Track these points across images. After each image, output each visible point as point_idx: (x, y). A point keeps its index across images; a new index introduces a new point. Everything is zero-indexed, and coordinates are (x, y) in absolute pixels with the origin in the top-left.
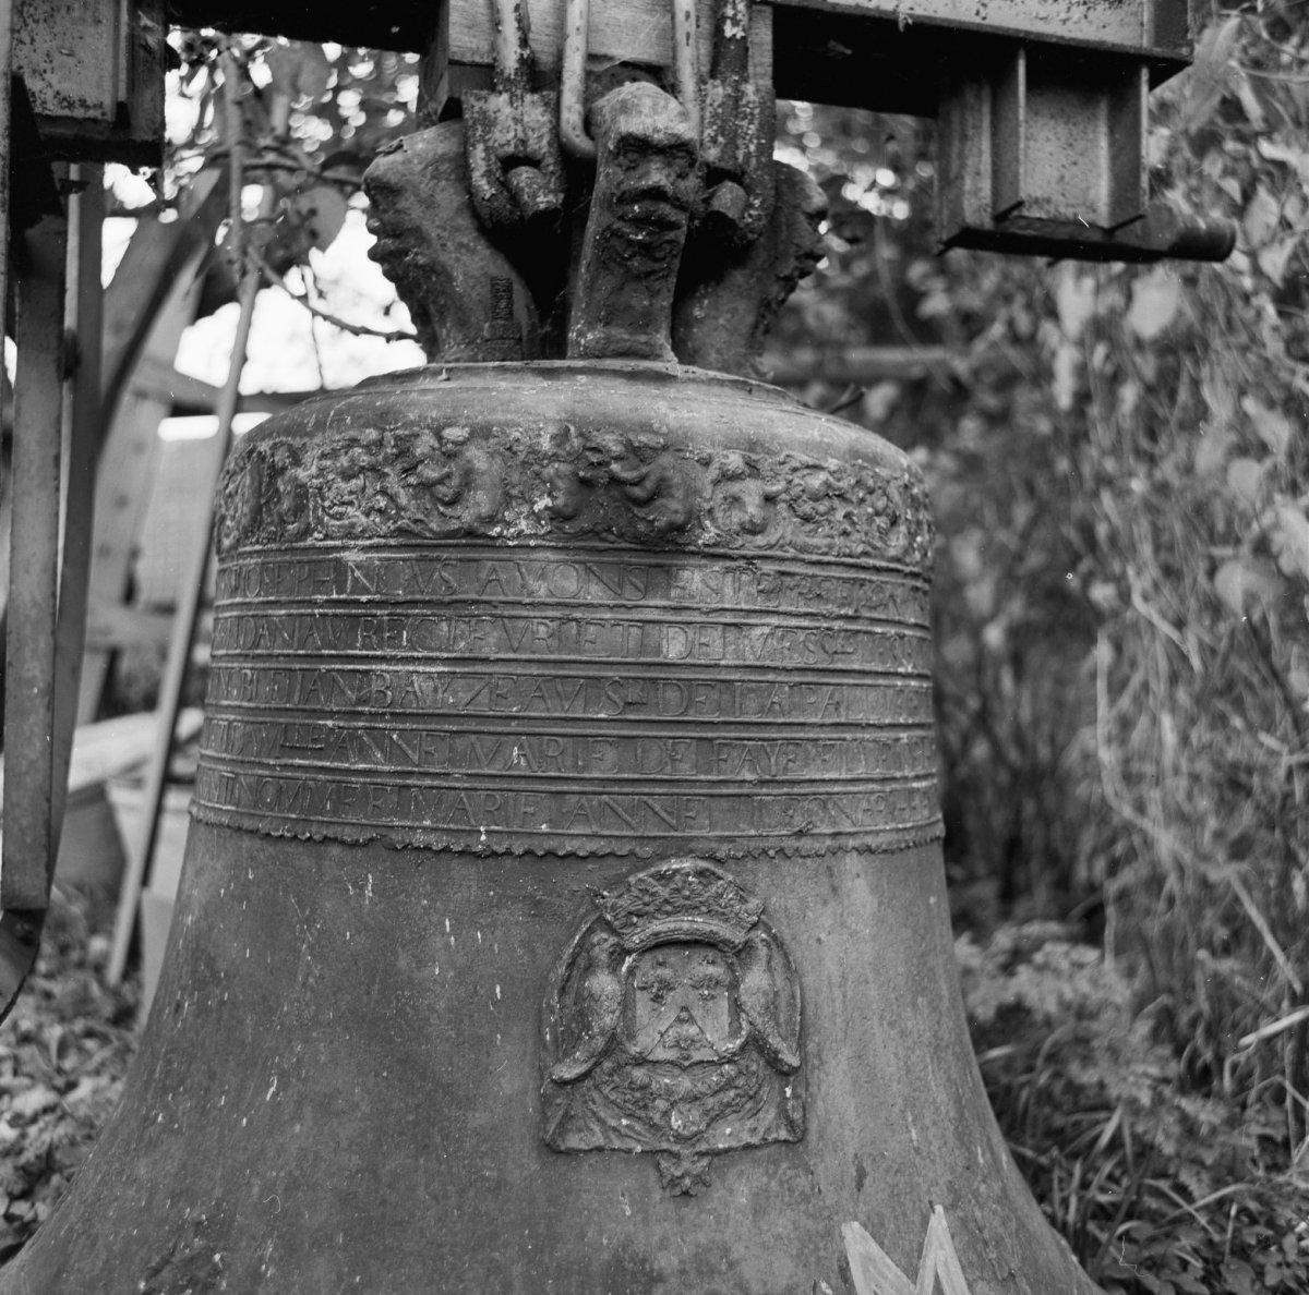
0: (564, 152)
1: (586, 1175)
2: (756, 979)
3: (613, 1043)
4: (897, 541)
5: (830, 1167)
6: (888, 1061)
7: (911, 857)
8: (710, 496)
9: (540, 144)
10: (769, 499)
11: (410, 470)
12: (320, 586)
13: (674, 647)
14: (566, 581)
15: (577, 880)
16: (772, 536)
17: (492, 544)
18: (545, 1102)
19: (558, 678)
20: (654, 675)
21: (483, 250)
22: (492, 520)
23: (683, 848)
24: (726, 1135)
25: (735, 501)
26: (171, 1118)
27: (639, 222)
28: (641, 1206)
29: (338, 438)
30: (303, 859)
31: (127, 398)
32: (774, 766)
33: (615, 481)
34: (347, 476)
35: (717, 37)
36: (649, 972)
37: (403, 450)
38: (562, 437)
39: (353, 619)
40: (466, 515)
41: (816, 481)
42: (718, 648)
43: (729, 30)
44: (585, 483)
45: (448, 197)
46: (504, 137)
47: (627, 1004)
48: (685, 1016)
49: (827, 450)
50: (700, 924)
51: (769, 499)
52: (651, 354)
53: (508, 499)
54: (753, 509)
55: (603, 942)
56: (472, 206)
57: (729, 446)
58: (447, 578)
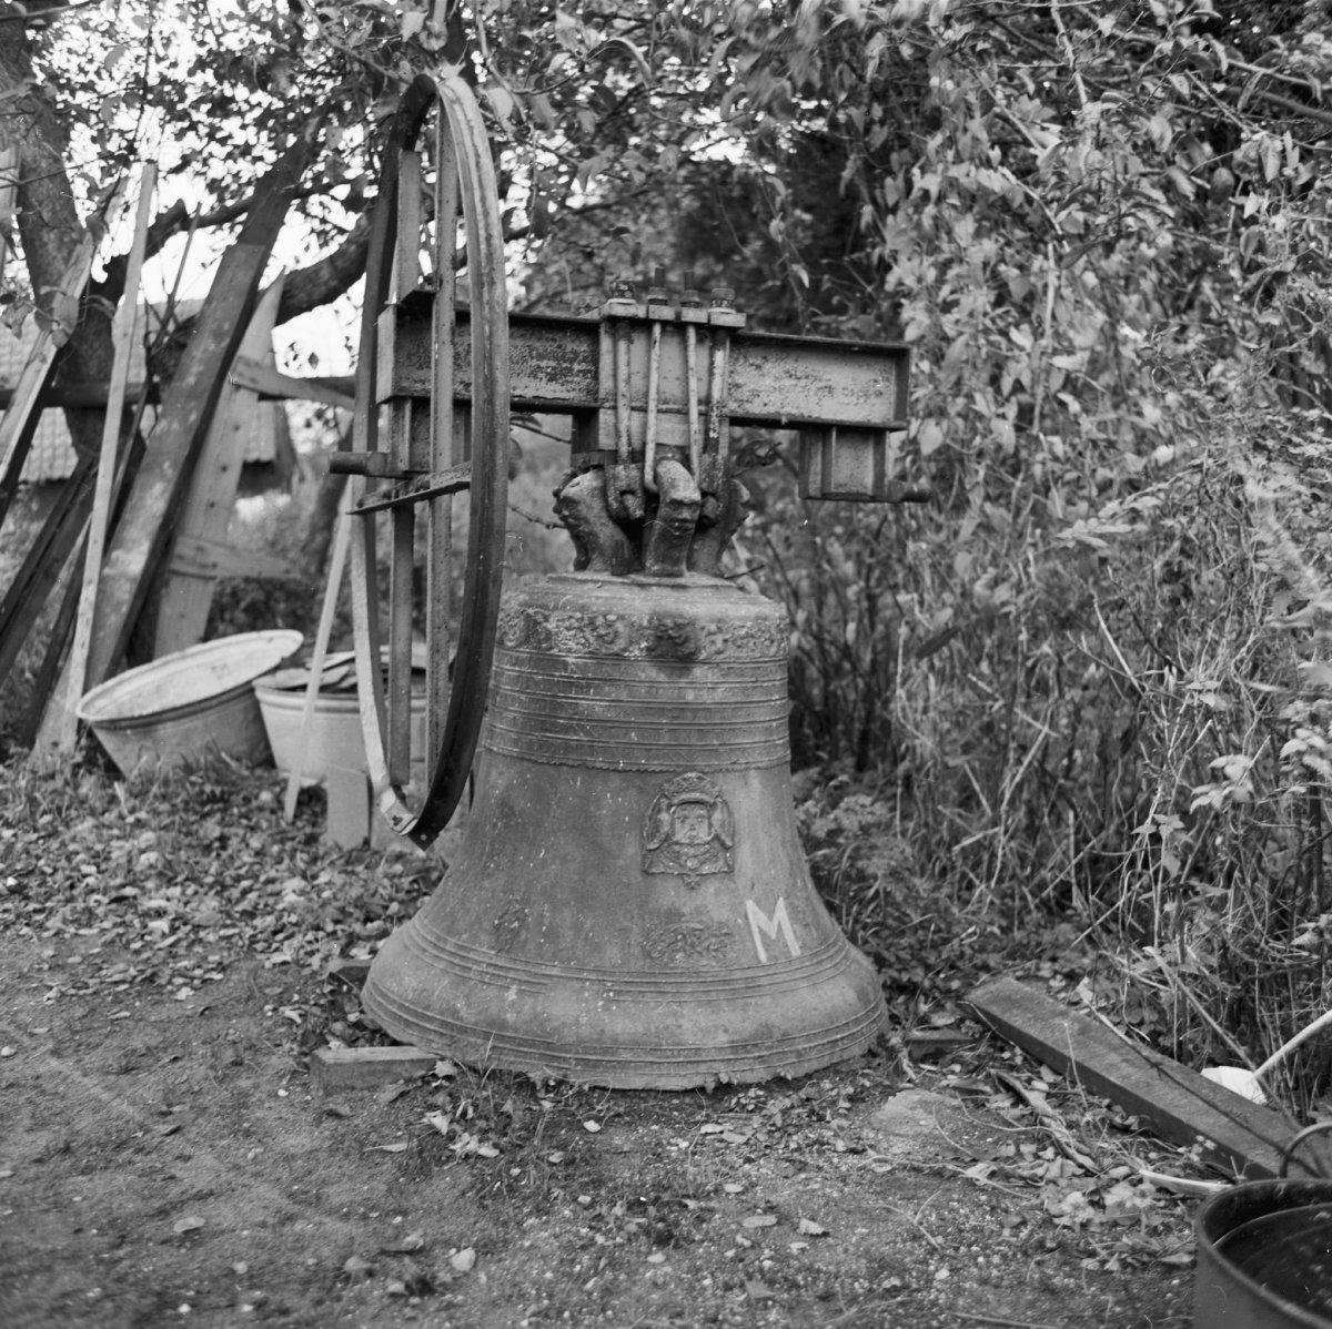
0: (646, 491)
1: (658, 881)
2: (717, 816)
3: (668, 837)
4: (773, 649)
5: (742, 881)
6: (764, 845)
7: (775, 771)
8: (704, 641)
9: (636, 486)
10: (726, 641)
11: (594, 629)
12: (556, 669)
13: (690, 696)
14: (651, 673)
15: (655, 780)
16: (727, 654)
17: (625, 659)
18: (644, 857)
19: (648, 709)
20: (682, 708)
21: (611, 525)
22: (625, 650)
23: (692, 769)
24: (706, 869)
25: (713, 642)
26: (498, 865)
27: (678, 529)
28: (677, 893)
29: (565, 615)
30: (551, 771)
31: (226, 388)
32: (726, 739)
33: (670, 637)
34: (568, 629)
35: (707, 439)
36: (680, 813)
37: (592, 622)
38: (650, 621)
39: (570, 685)
40: (616, 648)
41: (743, 632)
42: (707, 697)
43: (712, 435)
44: (660, 638)
45: (597, 505)
46: (622, 484)
47: (672, 824)
48: (692, 828)
49: (745, 618)
50: (697, 795)
51: (726, 641)
52: (680, 575)
53: (631, 643)
54: (719, 645)
55: (664, 802)
56: (607, 507)
57: (712, 621)
58: (607, 670)
